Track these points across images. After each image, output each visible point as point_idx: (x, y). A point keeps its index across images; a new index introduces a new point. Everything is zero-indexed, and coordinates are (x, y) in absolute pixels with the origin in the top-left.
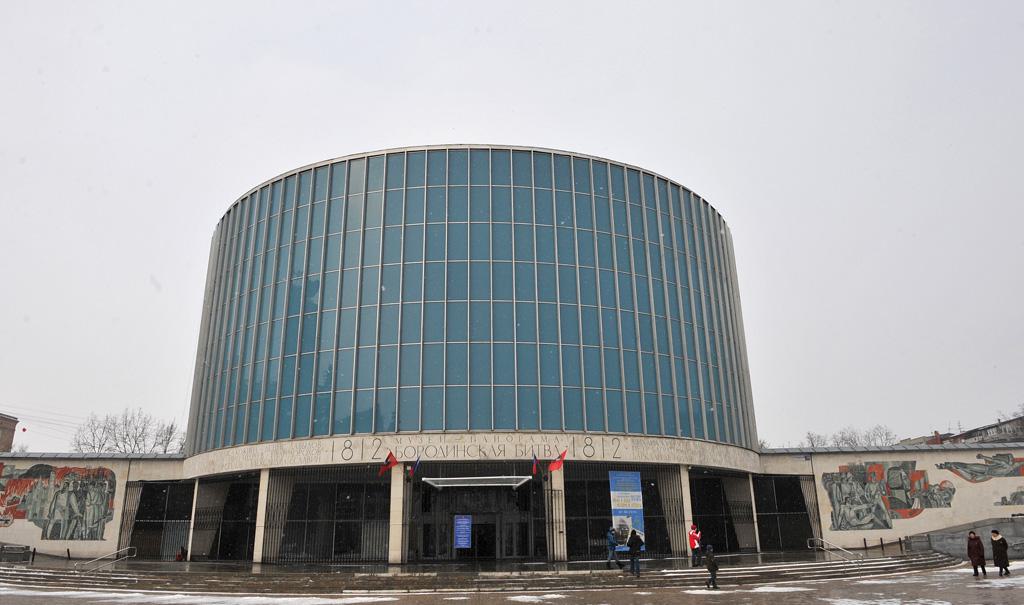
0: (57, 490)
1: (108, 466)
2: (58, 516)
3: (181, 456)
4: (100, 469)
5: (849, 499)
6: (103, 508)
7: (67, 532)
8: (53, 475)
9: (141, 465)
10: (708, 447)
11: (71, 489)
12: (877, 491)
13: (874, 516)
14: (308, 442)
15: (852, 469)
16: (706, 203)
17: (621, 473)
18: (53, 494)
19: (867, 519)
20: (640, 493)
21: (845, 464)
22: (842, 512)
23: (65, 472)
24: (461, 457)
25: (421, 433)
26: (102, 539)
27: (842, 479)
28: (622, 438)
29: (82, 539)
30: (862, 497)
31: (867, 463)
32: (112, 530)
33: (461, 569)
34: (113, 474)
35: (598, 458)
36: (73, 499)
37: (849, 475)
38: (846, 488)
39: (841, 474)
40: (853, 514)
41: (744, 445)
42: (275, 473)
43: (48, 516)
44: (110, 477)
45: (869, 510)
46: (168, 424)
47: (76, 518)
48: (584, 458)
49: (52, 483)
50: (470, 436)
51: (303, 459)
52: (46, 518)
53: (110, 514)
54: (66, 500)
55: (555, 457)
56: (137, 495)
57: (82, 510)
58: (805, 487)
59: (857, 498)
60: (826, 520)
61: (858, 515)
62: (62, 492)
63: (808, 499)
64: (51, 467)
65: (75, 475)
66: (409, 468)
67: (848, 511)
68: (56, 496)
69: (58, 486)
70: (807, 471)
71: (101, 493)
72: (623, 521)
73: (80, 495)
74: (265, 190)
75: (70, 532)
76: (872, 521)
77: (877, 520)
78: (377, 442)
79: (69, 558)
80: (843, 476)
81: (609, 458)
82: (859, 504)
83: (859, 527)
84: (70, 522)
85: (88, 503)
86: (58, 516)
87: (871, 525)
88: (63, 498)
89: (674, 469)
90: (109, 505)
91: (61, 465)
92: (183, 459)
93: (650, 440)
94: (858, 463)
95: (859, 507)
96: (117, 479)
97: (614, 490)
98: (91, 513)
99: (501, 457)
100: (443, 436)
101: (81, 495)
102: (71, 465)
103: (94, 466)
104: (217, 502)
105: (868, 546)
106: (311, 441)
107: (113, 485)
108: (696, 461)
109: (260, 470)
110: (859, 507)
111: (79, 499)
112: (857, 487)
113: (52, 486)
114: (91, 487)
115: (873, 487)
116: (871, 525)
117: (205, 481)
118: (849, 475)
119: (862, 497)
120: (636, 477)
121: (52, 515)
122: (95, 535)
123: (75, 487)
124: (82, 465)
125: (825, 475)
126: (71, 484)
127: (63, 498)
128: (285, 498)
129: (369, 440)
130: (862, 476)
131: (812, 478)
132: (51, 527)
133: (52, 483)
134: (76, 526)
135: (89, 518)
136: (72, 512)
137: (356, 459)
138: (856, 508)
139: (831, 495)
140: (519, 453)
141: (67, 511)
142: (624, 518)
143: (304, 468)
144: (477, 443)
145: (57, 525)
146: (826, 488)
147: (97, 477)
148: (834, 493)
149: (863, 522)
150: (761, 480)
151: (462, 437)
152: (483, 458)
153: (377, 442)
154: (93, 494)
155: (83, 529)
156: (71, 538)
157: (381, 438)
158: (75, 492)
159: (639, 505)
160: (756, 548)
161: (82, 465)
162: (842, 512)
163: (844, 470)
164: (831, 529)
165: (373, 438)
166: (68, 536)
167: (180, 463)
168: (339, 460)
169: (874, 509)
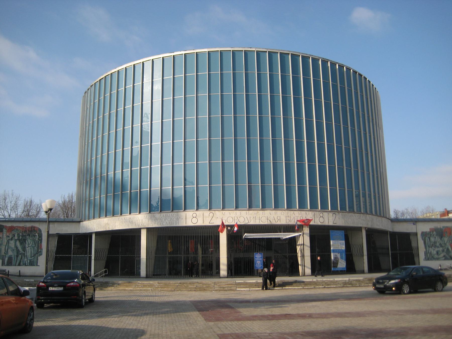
0: (8, 238)
1: (36, 225)
2: (10, 253)
3: (79, 220)
4: (32, 227)
5: (434, 245)
6: (36, 249)
7: (17, 261)
8: (4, 230)
9: (56, 224)
10: (375, 218)
11: (16, 238)
12: (447, 241)
13: (445, 254)
14: (170, 214)
15: (436, 230)
16: (365, 78)
17: (336, 231)
18: (6, 241)
19: (442, 255)
20: (344, 241)
22: (430, 251)
23: (11, 229)
24: (257, 222)
26: (37, 265)
27: (431, 235)
28: (337, 213)
29: (26, 265)
30: (440, 244)
31: (443, 227)
32: (42, 260)
33: (109, 282)
34: (40, 231)
35: (326, 223)
36: (18, 243)
37: (434, 233)
38: (432, 239)
39: (430, 232)
40: (435, 252)
41: (382, 215)
42: (149, 230)
43: (5, 253)
44: (38, 232)
45: (443, 251)
46: (29, 200)
47: (21, 254)
48: (319, 224)
49: (5, 235)
50: (274, 211)
51: (168, 222)
52: (3, 254)
53: (41, 252)
54: (14, 244)
55: (235, 224)
56: (54, 243)
57: (24, 249)
58: (412, 238)
59: (438, 244)
60: (422, 255)
61: (437, 253)
62: (12, 239)
63: (414, 244)
64: (3, 226)
65: (17, 230)
66: (229, 228)
67: (432, 251)
68: (8, 242)
69: (8, 237)
70: (414, 231)
71: (34, 240)
72: (336, 255)
73: (21, 242)
75: (18, 262)
76: (444, 256)
77: (447, 256)
78: (211, 214)
79: (20, 276)
80: (432, 233)
81: (331, 224)
82: (438, 247)
83: (438, 259)
84: (17, 256)
85: (27, 246)
86: (10, 253)
87: (444, 258)
88: (12, 243)
89: (359, 229)
90: (39, 247)
91: (9, 225)
92: (80, 222)
93: (350, 214)
94: (439, 227)
96: (42, 232)
97: (333, 240)
98: (29, 251)
99: (279, 223)
100: (248, 211)
101: (23, 242)
102: (15, 225)
103: (28, 225)
104: (106, 245)
105: (21, 275)
106: (173, 213)
107: (40, 236)
108: (370, 226)
111: (21, 244)
112: (438, 239)
113: (5, 236)
114: (28, 237)
115: (446, 239)
116: (444, 258)
117: (99, 234)
118: (434, 233)
119: (440, 244)
120: (342, 233)
121: (6, 252)
122: (32, 263)
123: (19, 237)
124: (22, 225)
125: (423, 233)
126: (16, 235)
127: (12, 243)
129: (207, 213)
130: (441, 233)
131: (416, 234)
132: (6, 259)
133: (5, 235)
134: (21, 258)
135: (29, 254)
136: (18, 251)
137: (200, 223)
138: (437, 249)
140: (288, 221)
141: (15, 250)
142: (337, 254)
143: (167, 227)
144: (266, 215)
145: (10, 258)
146: (423, 239)
147: (31, 231)
148: (427, 242)
149: (440, 256)
150: (394, 235)
151: (258, 212)
152: (269, 223)
153: (211, 214)
154: (29, 241)
155: (26, 260)
156: (19, 265)
157: (213, 212)
158: (19, 239)
159: (343, 248)
160: (390, 269)
161: (22, 225)
162: (430, 251)
163: (432, 230)
164: (424, 260)
165: (209, 212)
166: (17, 264)
167: (77, 224)
168: (207, 223)
169: (445, 250)
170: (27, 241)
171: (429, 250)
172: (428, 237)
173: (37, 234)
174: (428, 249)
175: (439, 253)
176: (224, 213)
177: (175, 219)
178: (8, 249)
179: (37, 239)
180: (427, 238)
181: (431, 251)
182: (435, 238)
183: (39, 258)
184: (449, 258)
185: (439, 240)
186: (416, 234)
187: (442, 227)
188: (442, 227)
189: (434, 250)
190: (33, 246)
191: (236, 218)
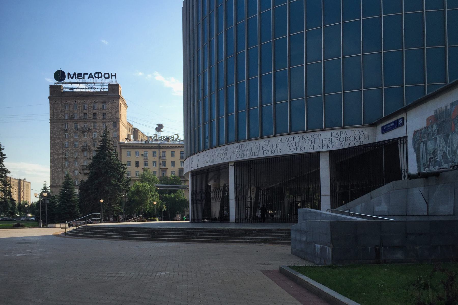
21: (433, 113)
180: (422, 144)
182: (436, 139)
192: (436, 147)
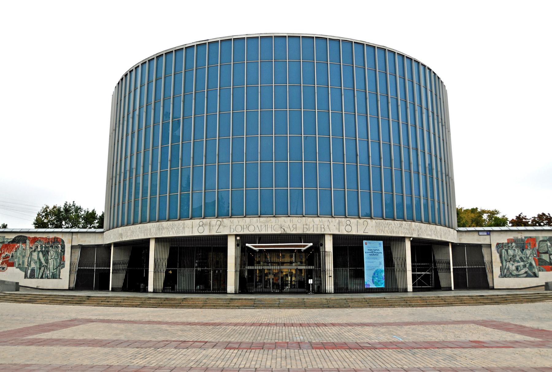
4: (55, 238)
13: (527, 270)
15: (515, 241)
25: (245, 217)
26: (59, 278)
34: (63, 242)
38: (511, 252)
40: (514, 268)
44: (61, 243)
45: (525, 266)
59: (518, 258)
67: (511, 266)
74: (151, 62)
77: (529, 272)
82: (518, 262)
95: (519, 264)
109: (325, 234)
110: (519, 264)
114: (50, 248)
128: (165, 255)
131: (490, 246)
139: (501, 256)
149: (520, 273)
154: (52, 252)
170: (49, 253)
171: (506, 265)
172: (505, 250)
173: (59, 246)
174: (504, 264)
175: (519, 268)
176: (232, 221)
177: (181, 228)
178: (30, 262)
179: (60, 251)
180: (504, 250)
181: (509, 266)
182: (515, 250)
183: (61, 270)
184: (532, 274)
185: (520, 253)
186: (490, 246)
187: (523, 238)
188: (523, 238)
189: (513, 265)
190: (56, 258)
191: (245, 227)
192: (515, 253)
